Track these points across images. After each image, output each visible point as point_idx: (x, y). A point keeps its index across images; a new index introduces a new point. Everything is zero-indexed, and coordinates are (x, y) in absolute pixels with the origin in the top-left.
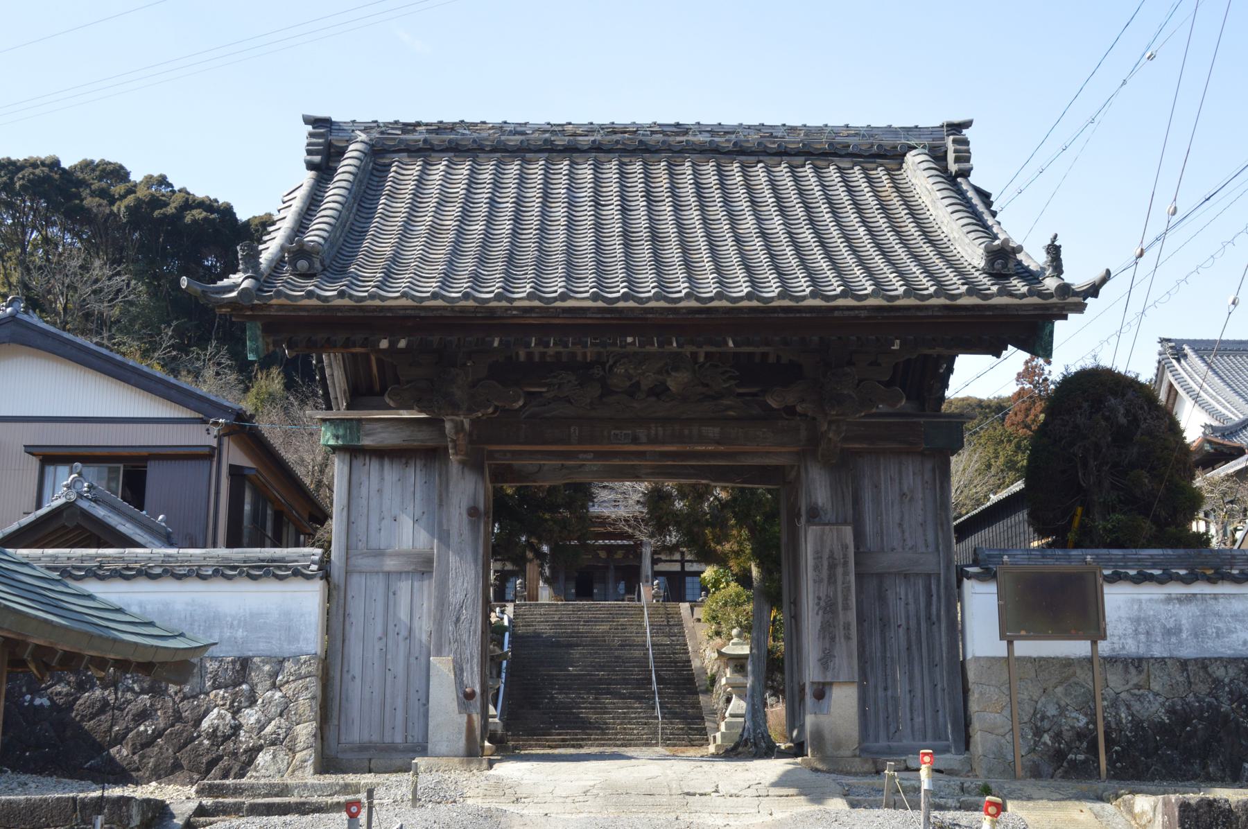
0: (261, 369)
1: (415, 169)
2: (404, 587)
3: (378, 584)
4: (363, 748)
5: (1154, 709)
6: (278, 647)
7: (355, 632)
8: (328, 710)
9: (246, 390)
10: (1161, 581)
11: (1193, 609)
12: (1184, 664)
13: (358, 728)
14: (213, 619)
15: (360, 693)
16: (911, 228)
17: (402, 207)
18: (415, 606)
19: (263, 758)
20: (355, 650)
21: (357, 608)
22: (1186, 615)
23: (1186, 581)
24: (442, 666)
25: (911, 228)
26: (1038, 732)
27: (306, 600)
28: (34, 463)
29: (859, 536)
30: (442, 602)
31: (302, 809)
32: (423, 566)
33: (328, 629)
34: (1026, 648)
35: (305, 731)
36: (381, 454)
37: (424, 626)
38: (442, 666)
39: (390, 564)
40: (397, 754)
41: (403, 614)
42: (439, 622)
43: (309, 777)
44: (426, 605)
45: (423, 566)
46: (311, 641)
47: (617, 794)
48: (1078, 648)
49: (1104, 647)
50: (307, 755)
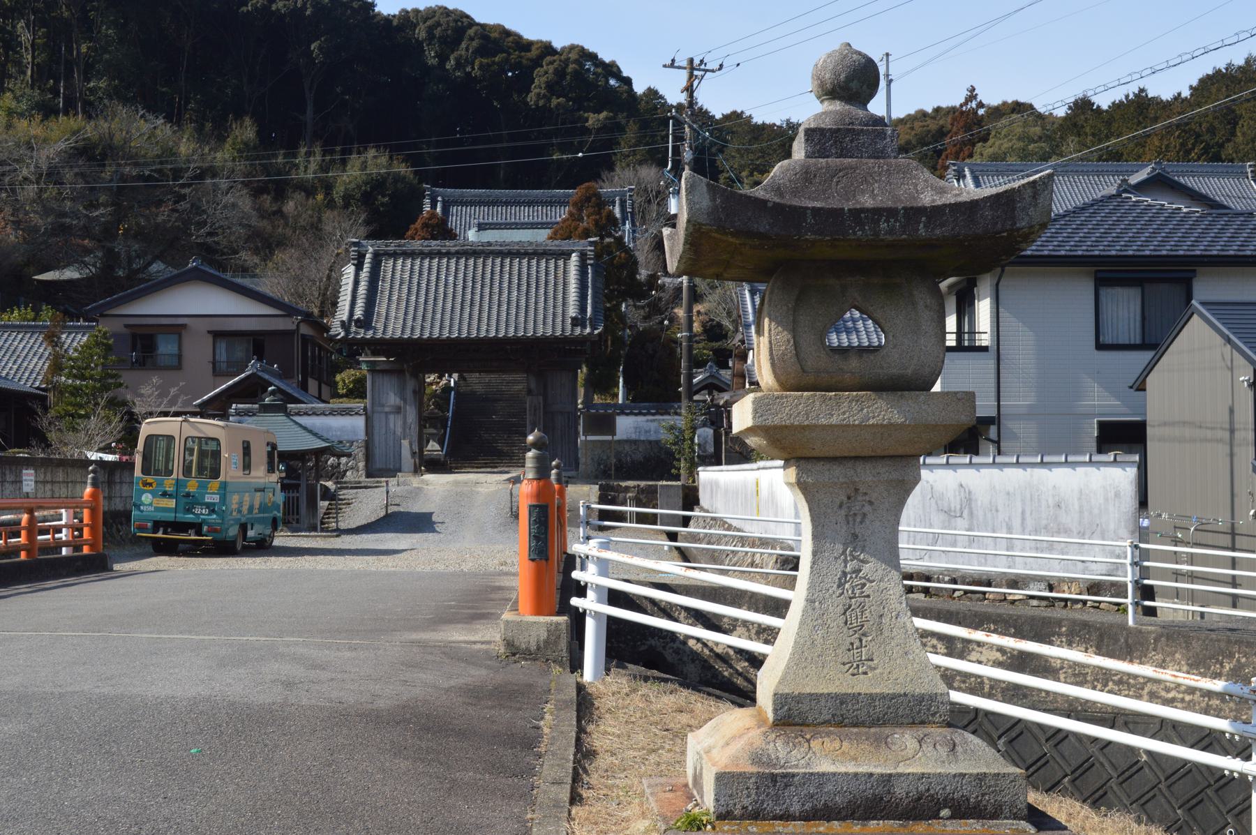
0: (236, 120)
1: (391, 262)
2: (392, 417)
3: (383, 416)
4: (380, 470)
5: (639, 457)
6: (351, 438)
7: (376, 431)
8: (368, 457)
9: (221, 139)
10: (644, 415)
11: (655, 424)
12: (650, 442)
13: (378, 465)
14: (329, 429)
15: (378, 452)
16: (560, 296)
17: (387, 285)
18: (395, 423)
19: (348, 473)
20: (376, 438)
21: (376, 424)
22: (653, 426)
23: (653, 414)
24: (405, 443)
25: (560, 296)
26: (599, 464)
27: (360, 422)
28: (210, 339)
29: (545, 400)
30: (405, 422)
31: (366, 487)
32: (398, 410)
33: (367, 434)
34: (589, 438)
35: (361, 465)
36: (383, 372)
37: (399, 430)
38: (405, 443)
39: (387, 409)
40: (392, 472)
41: (392, 426)
42: (404, 429)
43: (363, 479)
44: (399, 423)
45: (398, 410)
46: (362, 435)
47: (457, 483)
48: (609, 438)
49: (616, 438)
50: (362, 473)
